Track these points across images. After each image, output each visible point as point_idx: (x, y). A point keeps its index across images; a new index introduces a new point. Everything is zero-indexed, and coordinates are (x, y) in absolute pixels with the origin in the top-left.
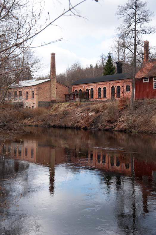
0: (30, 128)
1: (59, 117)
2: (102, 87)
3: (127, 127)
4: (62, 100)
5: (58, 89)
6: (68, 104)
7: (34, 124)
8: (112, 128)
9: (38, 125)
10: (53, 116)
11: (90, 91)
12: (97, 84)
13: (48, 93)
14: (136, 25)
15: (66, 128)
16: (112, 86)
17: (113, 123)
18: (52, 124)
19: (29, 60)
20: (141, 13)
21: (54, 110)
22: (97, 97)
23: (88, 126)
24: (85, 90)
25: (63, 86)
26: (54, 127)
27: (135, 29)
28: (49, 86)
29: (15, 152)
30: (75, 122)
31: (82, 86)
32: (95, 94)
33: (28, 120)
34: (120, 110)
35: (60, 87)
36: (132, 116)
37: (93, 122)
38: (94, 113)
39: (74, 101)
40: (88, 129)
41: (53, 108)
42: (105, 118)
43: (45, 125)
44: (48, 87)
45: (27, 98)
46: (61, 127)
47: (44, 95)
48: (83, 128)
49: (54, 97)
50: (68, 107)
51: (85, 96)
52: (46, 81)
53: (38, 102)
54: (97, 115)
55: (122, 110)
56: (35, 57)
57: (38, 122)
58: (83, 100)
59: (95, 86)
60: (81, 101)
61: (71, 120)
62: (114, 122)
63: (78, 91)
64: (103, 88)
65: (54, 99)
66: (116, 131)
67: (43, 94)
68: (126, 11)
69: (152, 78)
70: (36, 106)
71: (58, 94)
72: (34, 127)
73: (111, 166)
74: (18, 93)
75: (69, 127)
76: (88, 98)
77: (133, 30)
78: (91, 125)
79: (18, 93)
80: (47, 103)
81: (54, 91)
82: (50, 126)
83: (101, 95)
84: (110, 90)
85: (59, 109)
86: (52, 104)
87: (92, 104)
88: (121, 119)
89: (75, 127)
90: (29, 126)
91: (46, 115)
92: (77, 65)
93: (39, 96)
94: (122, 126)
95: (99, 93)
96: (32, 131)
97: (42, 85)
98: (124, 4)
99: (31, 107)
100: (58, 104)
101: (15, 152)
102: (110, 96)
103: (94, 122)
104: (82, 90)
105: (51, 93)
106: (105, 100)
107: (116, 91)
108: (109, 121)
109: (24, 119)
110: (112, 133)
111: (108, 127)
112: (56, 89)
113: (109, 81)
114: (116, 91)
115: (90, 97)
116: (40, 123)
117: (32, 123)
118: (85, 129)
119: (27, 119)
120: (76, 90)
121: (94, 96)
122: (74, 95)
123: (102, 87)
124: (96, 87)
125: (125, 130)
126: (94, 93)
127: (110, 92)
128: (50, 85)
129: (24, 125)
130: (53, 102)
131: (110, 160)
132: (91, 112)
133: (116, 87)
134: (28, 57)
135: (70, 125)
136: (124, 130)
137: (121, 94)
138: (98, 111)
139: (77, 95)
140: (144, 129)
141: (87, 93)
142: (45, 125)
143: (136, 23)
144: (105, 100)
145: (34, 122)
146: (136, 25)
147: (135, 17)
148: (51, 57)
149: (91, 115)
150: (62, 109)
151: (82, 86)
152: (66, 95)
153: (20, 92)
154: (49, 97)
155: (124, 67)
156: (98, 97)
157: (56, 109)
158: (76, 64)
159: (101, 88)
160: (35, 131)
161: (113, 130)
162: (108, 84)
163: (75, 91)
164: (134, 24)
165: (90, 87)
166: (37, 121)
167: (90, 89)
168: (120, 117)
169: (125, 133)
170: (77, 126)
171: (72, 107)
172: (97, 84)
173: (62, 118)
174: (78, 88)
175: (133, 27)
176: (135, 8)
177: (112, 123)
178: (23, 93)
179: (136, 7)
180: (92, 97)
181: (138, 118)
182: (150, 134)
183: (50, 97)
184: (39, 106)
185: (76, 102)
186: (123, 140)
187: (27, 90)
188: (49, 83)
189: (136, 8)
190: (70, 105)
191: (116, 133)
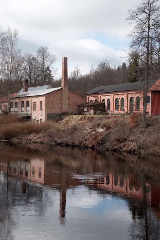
0: (35, 145)
1: (67, 133)
3: (136, 148)
4: (75, 111)
7: (39, 140)
8: (121, 148)
9: (43, 141)
10: (61, 131)
11: (106, 101)
12: (114, 94)
14: (149, 31)
15: (73, 146)
16: (130, 97)
18: (59, 141)
19: (45, 60)
20: (155, 17)
21: (64, 124)
26: (61, 144)
27: (149, 35)
28: (60, 96)
29: (21, 173)
30: (84, 139)
32: (112, 105)
33: (33, 136)
38: (105, 129)
41: (63, 121)
42: (113, 136)
46: (67, 145)
47: (54, 106)
49: (65, 108)
50: (79, 120)
54: (107, 132)
56: (52, 57)
59: (112, 96)
60: (95, 114)
61: (79, 137)
62: (123, 141)
64: (120, 99)
65: (65, 110)
66: (125, 152)
67: (52, 105)
68: (137, 16)
71: (71, 104)
72: (39, 144)
73: (129, 190)
74: (25, 103)
76: (105, 109)
77: (146, 37)
79: (25, 103)
80: (57, 115)
81: (66, 101)
82: (57, 144)
83: (118, 107)
84: (129, 102)
85: (70, 122)
87: (106, 117)
89: (82, 146)
90: (34, 142)
91: (52, 130)
92: (105, 64)
93: (48, 107)
95: (116, 104)
96: (38, 148)
98: (135, 9)
99: (39, 121)
101: (21, 173)
103: (103, 140)
105: (62, 104)
108: (118, 140)
110: (121, 154)
111: (116, 147)
118: (93, 148)
120: (91, 100)
121: (111, 108)
125: (134, 150)
128: (62, 94)
131: (128, 184)
132: (102, 128)
133: (136, 98)
134: (43, 57)
135: (77, 142)
136: (133, 151)
138: (109, 127)
140: (154, 151)
141: (103, 103)
142: (51, 142)
143: (149, 30)
144: (122, 112)
145: (40, 138)
146: (149, 31)
147: (148, 22)
149: (101, 132)
153: (28, 102)
154: (60, 108)
155: (53, 111)
158: (104, 63)
159: (119, 98)
161: (122, 150)
164: (147, 30)
165: (106, 98)
166: (43, 137)
167: (107, 99)
169: (134, 154)
171: (84, 121)
172: (114, 94)
175: (145, 34)
176: (148, 12)
177: (121, 142)
178: (30, 104)
179: (150, 11)
181: (149, 137)
182: (159, 156)
186: (133, 162)
187: (35, 100)
188: (60, 92)
189: (149, 12)
190: (82, 118)
191: (125, 154)
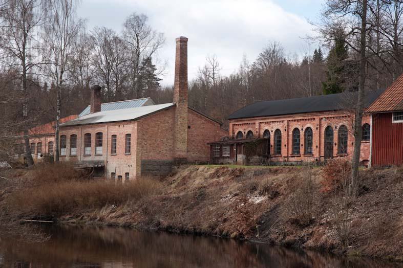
0: (112, 231)
1: (184, 206)
2: (337, 124)
3: (337, 241)
4: (204, 156)
5: (192, 129)
6: (213, 168)
7: (121, 221)
8: (302, 240)
9: (130, 224)
11: (272, 135)
12: (261, 121)
13: (168, 139)
15: (197, 234)
17: (304, 228)
18: (165, 223)
19: (140, 44)
21: (179, 185)
22: (290, 152)
23: (247, 234)
24: (262, 132)
25: (206, 120)
26: (169, 230)
31: (253, 122)
32: (286, 143)
34: (326, 194)
35: (199, 122)
36: (352, 213)
37: (259, 223)
38: (266, 197)
39: (230, 161)
40: (246, 240)
41: (176, 178)
42: (286, 214)
43: (148, 224)
44: (167, 124)
45: (114, 151)
46: (184, 232)
48: (236, 236)
49: (181, 149)
50: (212, 176)
51: (261, 149)
52: (159, 111)
53: (140, 163)
54: (272, 204)
55: (330, 194)
57: (133, 216)
58: (256, 158)
59: (286, 123)
60: (248, 162)
61: (210, 213)
62: (308, 225)
63: (245, 135)
64: (304, 129)
66: (311, 249)
69: (391, 113)
70: (133, 173)
72: (121, 230)
75: (202, 231)
76: (269, 153)
78: (253, 230)
81: (183, 135)
82: (160, 230)
84: (323, 136)
86: (176, 168)
88: (327, 217)
89: (216, 234)
92: (274, 52)
93: (143, 147)
94: (324, 237)
96: (118, 237)
97: (151, 118)
100: (192, 167)
102: (323, 154)
103: (263, 222)
104: (254, 133)
105: (174, 140)
106: (309, 160)
107: (336, 139)
108: (295, 222)
109: (101, 207)
110: (302, 253)
112: (186, 130)
113: (320, 112)
114: (336, 139)
115: (272, 151)
116: (139, 219)
117: (117, 217)
118: (240, 239)
119: (108, 207)
120: (240, 133)
121: (284, 151)
122: (232, 145)
123: (302, 126)
124: (288, 125)
125: (333, 247)
126: (284, 141)
127: (323, 140)
128: (174, 118)
129: (100, 222)
130: (181, 162)
132: (261, 194)
134: (137, 36)
135: (205, 226)
137: (348, 148)
139: (239, 145)
141: (264, 140)
144: (309, 160)
145: (123, 215)
148: (176, 49)
149: (258, 204)
150: (197, 182)
151: (253, 122)
152: (212, 145)
153: (99, 135)
156: (293, 152)
157: (185, 180)
158: (272, 49)
159: (300, 129)
160: (125, 240)
161: (304, 245)
162: (317, 120)
163: (236, 134)
168: (324, 211)
169: (333, 255)
170: (221, 231)
171: (222, 178)
172: (261, 121)
173: (191, 208)
174: (272, 124)
177: (303, 227)
180: (279, 151)
181: (367, 218)
183: (173, 149)
184: (142, 173)
185: (236, 163)
188: (170, 114)
190: (217, 171)
191: (311, 254)
